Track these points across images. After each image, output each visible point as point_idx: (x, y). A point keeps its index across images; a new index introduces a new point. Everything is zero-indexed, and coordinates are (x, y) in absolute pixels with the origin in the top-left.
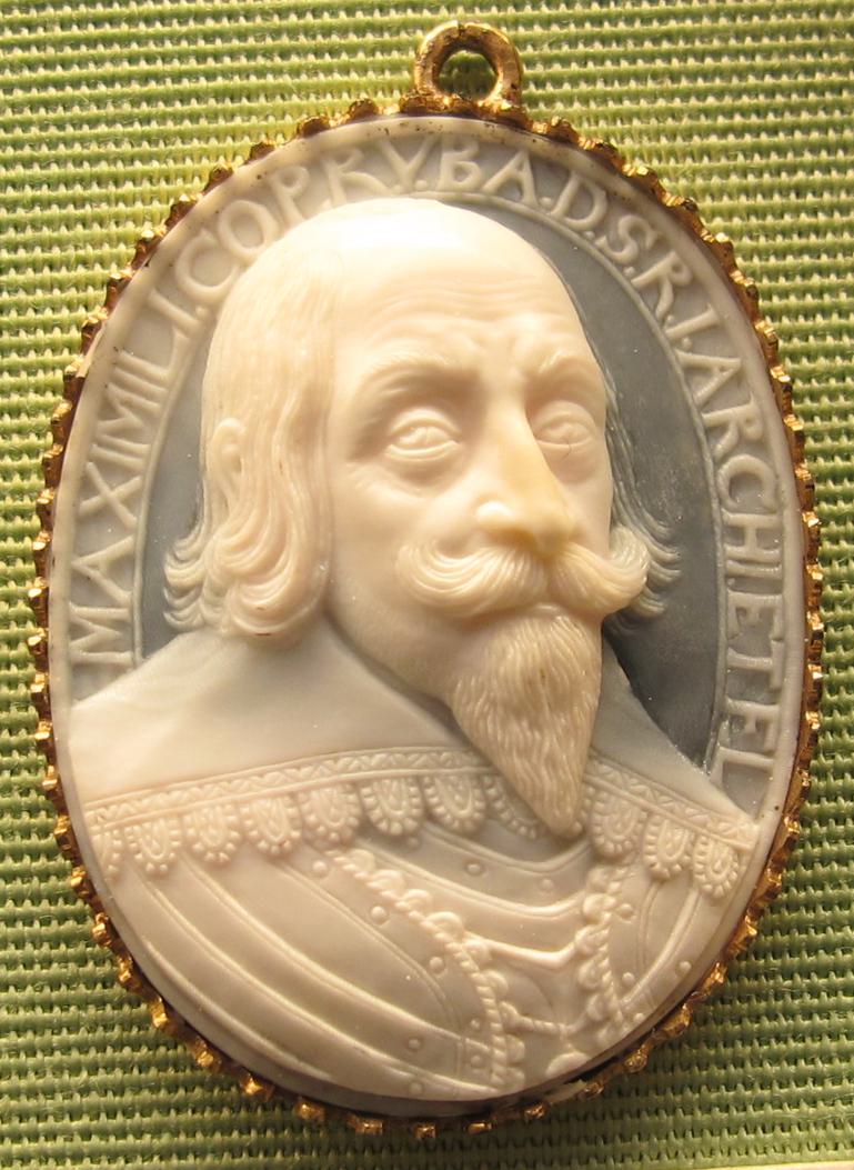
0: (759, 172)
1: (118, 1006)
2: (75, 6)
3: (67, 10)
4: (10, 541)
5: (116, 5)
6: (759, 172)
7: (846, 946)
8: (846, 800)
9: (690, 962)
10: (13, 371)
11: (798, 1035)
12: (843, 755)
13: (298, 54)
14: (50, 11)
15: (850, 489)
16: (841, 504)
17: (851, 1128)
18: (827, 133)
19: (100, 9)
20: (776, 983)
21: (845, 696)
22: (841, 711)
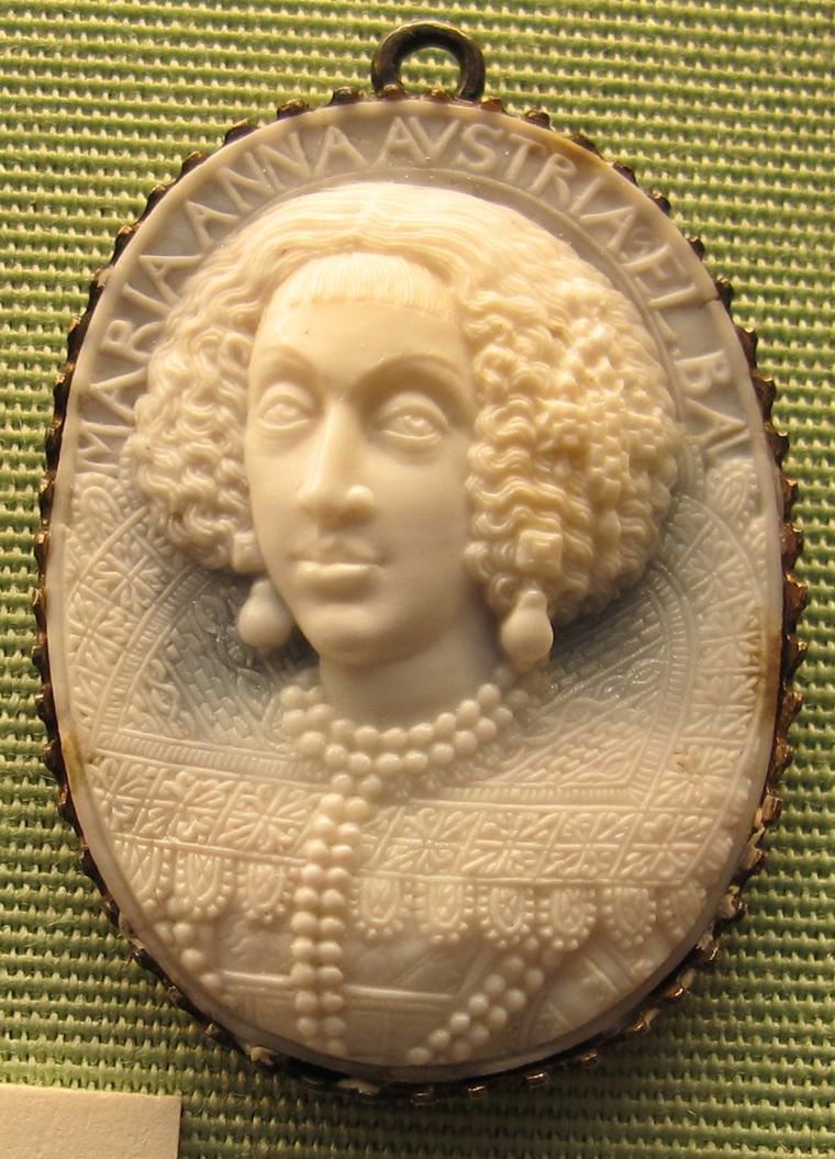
0: (39, 844)
1: (34, 780)
2: (212, 4)
3: (203, 8)
4: (12, 387)
5: (219, 7)
6: (39, 844)
7: (828, 974)
8: (827, 937)
9: (657, 918)
10: (12, 223)
11: (762, 1120)
12: (825, 708)
13: (97, 15)
14: (186, 7)
15: (833, 966)
16: (823, 584)
17: (831, 958)
18: (789, 265)
19: (235, 11)
20: (749, 938)
21: (828, 814)
22: (824, 788)
